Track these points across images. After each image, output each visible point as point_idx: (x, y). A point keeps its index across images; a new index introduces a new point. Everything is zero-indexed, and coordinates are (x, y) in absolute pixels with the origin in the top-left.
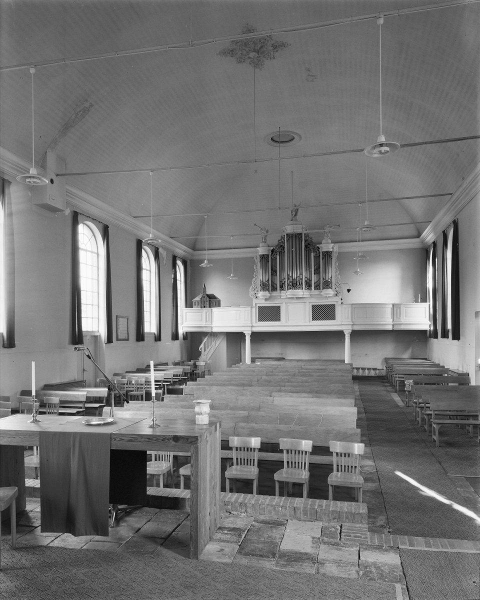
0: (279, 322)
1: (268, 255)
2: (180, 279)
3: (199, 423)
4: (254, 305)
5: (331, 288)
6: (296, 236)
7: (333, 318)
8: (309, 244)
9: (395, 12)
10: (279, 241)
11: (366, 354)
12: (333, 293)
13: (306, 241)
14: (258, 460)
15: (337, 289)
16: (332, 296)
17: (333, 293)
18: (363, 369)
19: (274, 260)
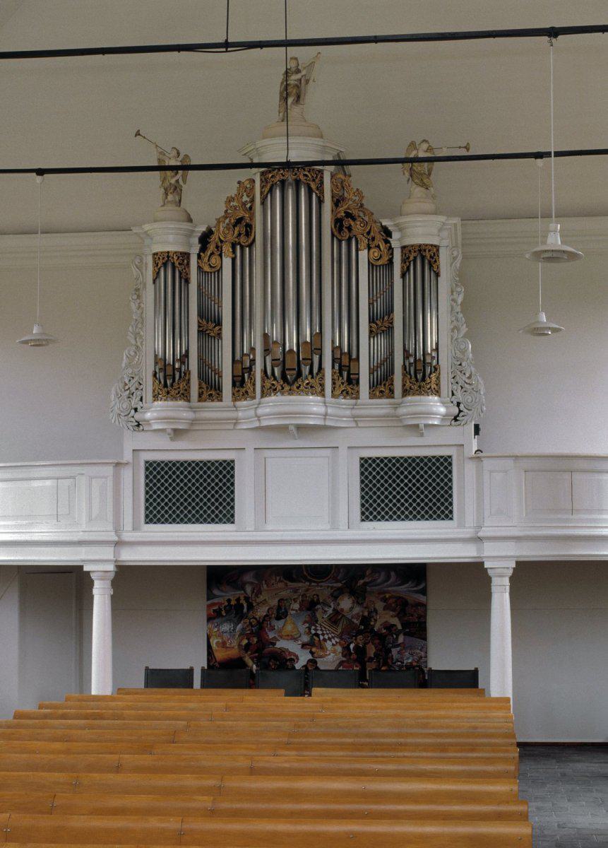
1: (185, 256)
4: (128, 456)
8: (348, 215)
12: (442, 410)
15: (459, 396)
17: (442, 410)
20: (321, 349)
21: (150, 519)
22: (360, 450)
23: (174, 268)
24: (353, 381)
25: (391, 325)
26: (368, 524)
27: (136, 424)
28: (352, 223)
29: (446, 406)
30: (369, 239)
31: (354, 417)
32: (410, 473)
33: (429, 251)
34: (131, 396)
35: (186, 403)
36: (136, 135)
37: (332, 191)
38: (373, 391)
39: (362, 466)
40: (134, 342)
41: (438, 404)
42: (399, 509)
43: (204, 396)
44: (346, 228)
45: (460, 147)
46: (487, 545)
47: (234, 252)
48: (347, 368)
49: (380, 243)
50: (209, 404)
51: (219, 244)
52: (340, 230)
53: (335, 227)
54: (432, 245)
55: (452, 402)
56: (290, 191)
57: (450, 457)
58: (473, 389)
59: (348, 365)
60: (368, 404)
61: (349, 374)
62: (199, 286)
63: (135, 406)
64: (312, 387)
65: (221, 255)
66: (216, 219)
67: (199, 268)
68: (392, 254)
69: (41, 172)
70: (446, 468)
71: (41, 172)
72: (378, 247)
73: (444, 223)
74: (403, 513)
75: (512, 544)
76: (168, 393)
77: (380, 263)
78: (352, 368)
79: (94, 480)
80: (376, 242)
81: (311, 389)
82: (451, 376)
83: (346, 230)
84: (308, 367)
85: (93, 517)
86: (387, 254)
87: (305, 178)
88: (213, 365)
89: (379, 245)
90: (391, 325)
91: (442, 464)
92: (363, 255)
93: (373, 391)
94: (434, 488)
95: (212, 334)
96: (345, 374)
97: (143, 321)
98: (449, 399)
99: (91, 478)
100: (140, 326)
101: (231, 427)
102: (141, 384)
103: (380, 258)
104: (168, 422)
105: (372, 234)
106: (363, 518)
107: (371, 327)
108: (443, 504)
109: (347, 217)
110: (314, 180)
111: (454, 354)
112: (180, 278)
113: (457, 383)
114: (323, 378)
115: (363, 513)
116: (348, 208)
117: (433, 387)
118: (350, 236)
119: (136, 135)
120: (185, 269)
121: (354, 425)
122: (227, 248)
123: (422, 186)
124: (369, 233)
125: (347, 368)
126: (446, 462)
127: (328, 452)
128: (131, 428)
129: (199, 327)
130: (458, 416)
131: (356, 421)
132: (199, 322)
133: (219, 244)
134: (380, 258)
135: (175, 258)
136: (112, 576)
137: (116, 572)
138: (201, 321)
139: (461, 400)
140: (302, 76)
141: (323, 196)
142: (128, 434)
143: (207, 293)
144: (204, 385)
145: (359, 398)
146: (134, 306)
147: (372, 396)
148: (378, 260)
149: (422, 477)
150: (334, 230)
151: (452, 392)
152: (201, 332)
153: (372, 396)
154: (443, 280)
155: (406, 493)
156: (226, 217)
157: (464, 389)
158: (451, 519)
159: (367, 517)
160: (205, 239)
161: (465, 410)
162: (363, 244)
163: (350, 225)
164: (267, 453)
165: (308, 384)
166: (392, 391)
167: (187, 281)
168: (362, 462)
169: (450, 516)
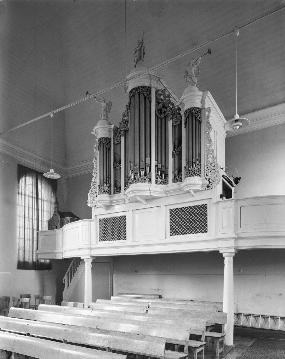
1: (110, 139)
2: (41, 209)
5: (199, 175)
6: (139, 93)
7: (203, 228)
8: (164, 107)
9: (173, 59)
11: (280, 295)
13: (158, 103)
14: (234, 326)
15: (210, 176)
16: (199, 188)
17: (201, 183)
18: (274, 318)
19: (117, 145)
21: (101, 240)
22: (169, 206)
25: (181, 150)
26: (173, 236)
28: (165, 110)
33: (195, 110)
36: (87, 94)
39: (171, 213)
44: (163, 112)
45: (206, 53)
48: (160, 169)
50: (117, 194)
52: (161, 113)
53: (158, 112)
55: (206, 179)
60: (171, 186)
64: (144, 179)
67: (114, 143)
68: (182, 119)
72: (176, 117)
76: (101, 191)
77: (177, 124)
78: (162, 169)
82: (206, 167)
89: (176, 116)
90: (181, 150)
96: (163, 175)
106: (171, 234)
108: (203, 226)
110: (146, 92)
112: (106, 148)
115: (171, 232)
119: (87, 94)
120: (108, 144)
121: (166, 196)
125: (160, 169)
127: (157, 208)
130: (209, 185)
131: (166, 194)
136: (233, 255)
137: (236, 254)
141: (151, 99)
145: (168, 184)
152: (115, 168)
157: (211, 172)
166: (181, 179)
168: (171, 211)
169: (206, 231)
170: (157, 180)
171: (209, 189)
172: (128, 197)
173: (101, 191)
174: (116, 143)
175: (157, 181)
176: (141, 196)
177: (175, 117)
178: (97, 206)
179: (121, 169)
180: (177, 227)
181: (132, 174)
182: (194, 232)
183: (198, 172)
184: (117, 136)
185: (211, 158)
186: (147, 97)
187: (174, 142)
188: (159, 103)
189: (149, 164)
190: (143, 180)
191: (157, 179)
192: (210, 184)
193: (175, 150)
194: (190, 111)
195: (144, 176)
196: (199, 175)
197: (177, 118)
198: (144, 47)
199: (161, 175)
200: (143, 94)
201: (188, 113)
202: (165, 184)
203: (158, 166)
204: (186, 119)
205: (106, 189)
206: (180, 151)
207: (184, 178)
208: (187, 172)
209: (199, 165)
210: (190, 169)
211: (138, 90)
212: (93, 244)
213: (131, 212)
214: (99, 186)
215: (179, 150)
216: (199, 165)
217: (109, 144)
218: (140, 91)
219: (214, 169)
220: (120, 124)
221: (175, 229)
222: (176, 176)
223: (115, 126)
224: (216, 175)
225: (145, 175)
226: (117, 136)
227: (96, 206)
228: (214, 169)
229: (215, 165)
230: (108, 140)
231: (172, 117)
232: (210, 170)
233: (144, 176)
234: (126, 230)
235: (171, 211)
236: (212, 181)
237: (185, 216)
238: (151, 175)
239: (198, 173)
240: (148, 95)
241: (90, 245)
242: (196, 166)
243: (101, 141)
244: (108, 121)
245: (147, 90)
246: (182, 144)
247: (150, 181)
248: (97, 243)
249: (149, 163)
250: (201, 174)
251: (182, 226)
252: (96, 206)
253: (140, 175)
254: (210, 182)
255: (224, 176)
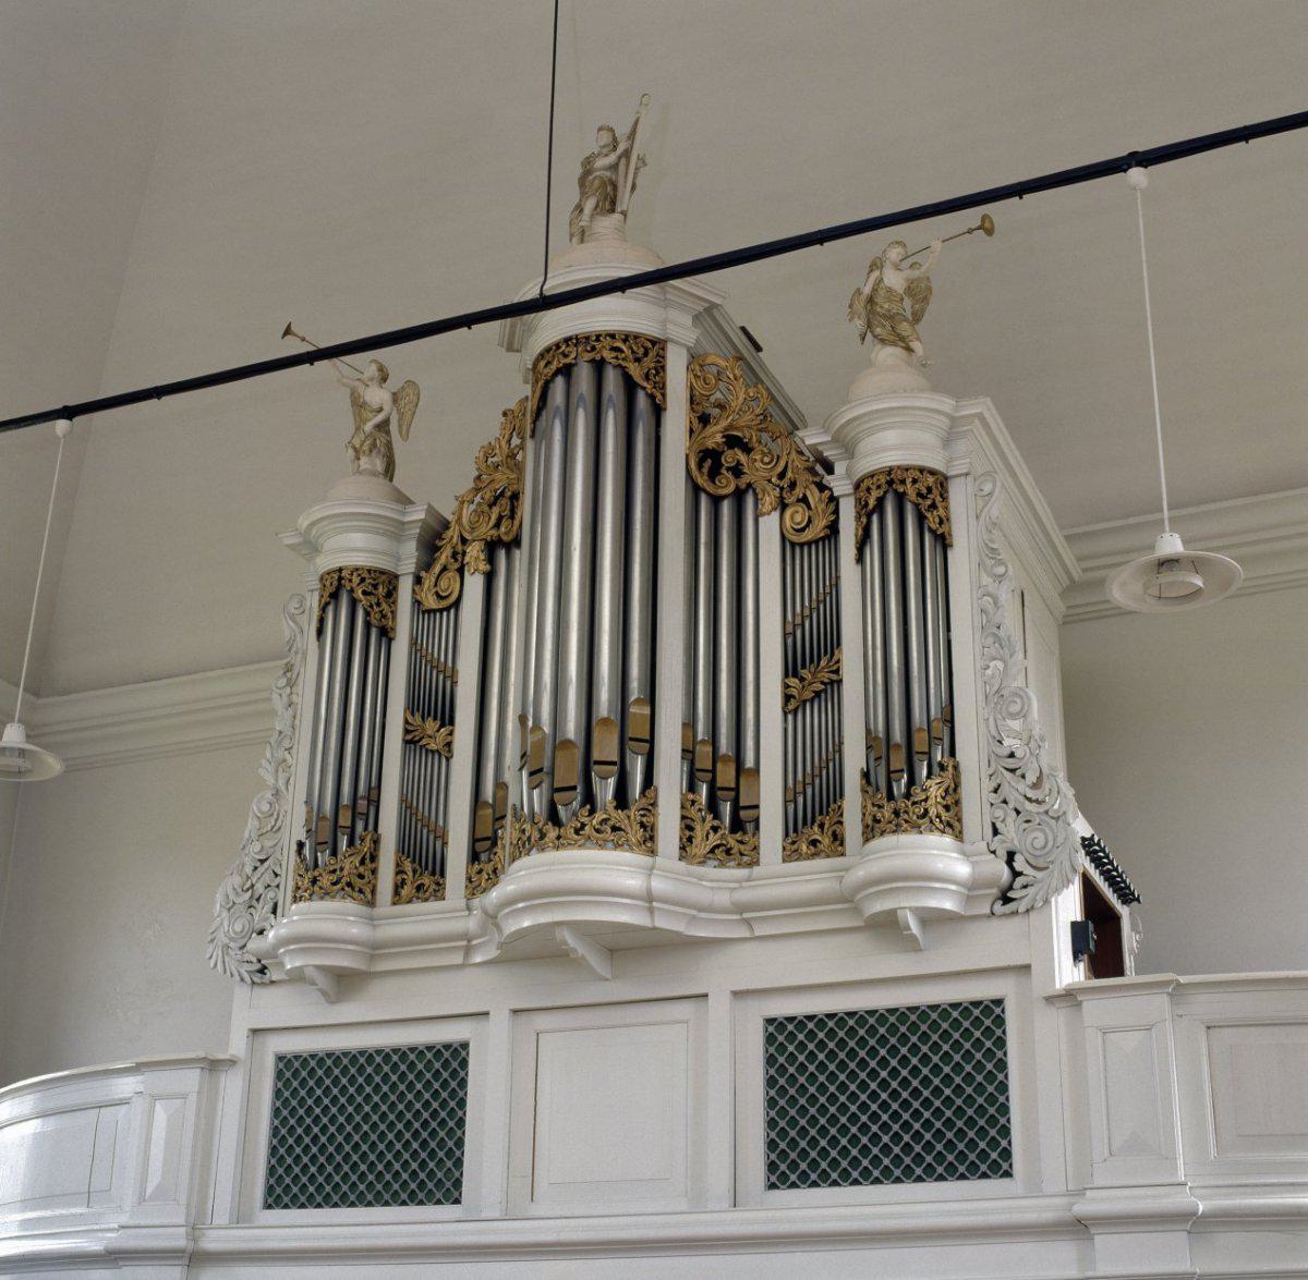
0: (447, 1211)
1: (392, 580)
3: (180, 1268)
4: (237, 1045)
5: (952, 824)
6: (599, 366)
8: (733, 441)
10: (488, 452)
12: (962, 869)
15: (1011, 832)
17: (962, 869)
20: (651, 741)
21: (277, 1197)
23: (353, 603)
24: (744, 822)
25: (834, 677)
26: (785, 1196)
27: (258, 966)
28: (743, 458)
29: (972, 863)
30: (782, 489)
31: (740, 908)
32: (893, 1051)
33: (915, 481)
34: (254, 903)
35: (364, 909)
37: (692, 389)
38: (794, 843)
39: (770, 1039)
40: (270, 780)
41: (955, 855)
42: (865, 1150)
43: (404, 892)
44: (728, 469)
45: (970, 231)
46: (1103, 1241)
47: (491, 560)
49: (808, 494)
51: (460, 548)
52: (714, 474)
53: (700, 466)
54: (922, 470)
55: (994, 852)
56: (611, 414)
57: (999, 1002)
58: (1047, 812)
59: (733, 785)
61: (736, 809)
62: (414, 642)
63: (258, 927)
64: (615, 829)
65: (461, 571)
66: (457, 498)
67: (417, 603)
68: (836, 512)
69: (69, 413)
70: (988, 1032)
71: (69, 413)
72: (804, 500)
73: (953, 419)
74: (876, 1161)
75: (1178, 1238)
76: (314, 881)
77: (808, 536)
79: (157, 1103)
80: (799, 492)
81: (614, 835)
83: (729, 475)
84: (612, 781)
85: (149, 1191)
86: (824, 512)
87: (614, 354)
88: (433, 818)
89: (805, 496)
90: (834, 677)
91: (977, 1022)
92: (770, 526)
93: (794, 843)
94: (958, 1090)
95: (433, 746)
96: (727, 808)
97: (294, 734)
98: (983, 845)
99: (155, 1098)
100: (286, 744)
101: (458, 959)
102: (276, 875)
103: (807, 525)
104: (302, 950)
105: (789, 474)
106: (773, 1179)
107: (786, 686)
109: (731, 447)
110: (638, 360)
111: (994, 732)
112: (368, 625)
113: (1005, 802)
114: (651, 808)
116: (731, 427)
117: (932, 812)
118: (737, 487)
120: (378, 604)
122: (475, 552)
123: (894, 344)
124: (782, 476)
126: (990, 1014)
128: (246, 977)
129: (407, 732)
132: (406, 722)
133: (460, 548)
134: (807, 525)
135: (356, 580)
138: (410, 719)
139: (1016, 845)
140: (620, 158)
141: (664, 395)
142: (242, 993)
143: (429, 658)
144: (408, 866)
145: (757, 863)
146: (279, 704)
147: (791, 853)
148: (803, 530)
149: (925, 1059)
150: (695, 472)
151: (994, 825)
152: (411, 741)
153: (791, 853)
154: (961, 559)
155: (884, 1106)
156: (477, 490)
157: (1022, 817)
158: (1008, 1174)
159: (783, 1178)
160: (432, 541)
161: (1028, 870)
162: (769, 500)
163: (739, 463)
164: (542, 1021)
165: (605, 821)
166: (838, 838)
167: (386, 634)
168: (771, 1029)
169: (1005, 1166)
170: (690, 839)
171: (1015, 913)
172: (498, 926)
173: (314, 881)
174: (431, 602)
175: (686, 843)
176: (583, 929)
177: (799, 500)
178: (273, 974)
179: (450, 751)
180: (328, 1082)
181: (536, 792)
182: (924, 1171)
183: (947, 808)
184: (437, 569)
185: (1017, 736)
186: (644, 388)
187: (790, 629)
188: (704, 420)
189: (707, 771)
190: (608, 835)
191: (690, 828)
192: (1020, 881)
193: (795, 674)
194: (890, 483)
195: (616, 808)
196: (950, 825)
197: (809, 508)
198: (642, 161)
199: (713, 807)
200: (619, 371)
201: (875, 494)
202: (739, 865)
203: (693, 752)
204: (864, 520)
205: (350, 864)
206: (832, 682)
207: (861, 839)
208: (880, 807)
209: (950, 768)
210: (899, 787)
211: (593, 348)
212: (217, 1221)
213: (500, 1022)
214: (301, 845)
215: (826, 676)
216: (950, 768)
217: (384, 606)
218: (608, 355)
219: (1037, 801)
220: (462, 503)
221: (376, 1099)
222: (805, 823)
223: (430, 510)
224: (1050, 838)
225: (622, 799)
226: (437, 569)
227: (262, 971)
228: (1037, 801)
229: (1040, 778)
230: (382, 583)
231: (782, 498)
232: (1011, 805)
233: (616, 808)
234: (274, 1136)
235: (771, 1029)
236: (1028, 870)
237: (863, 1064)
238: (654, 804)
239: (945, 815)
240: (647, 377)
241: (195, 1228)
242: (929, 776)
243: (339, 587)
244: (391, 480)
245: (646, 354)
246: (839, 644)
247: (652, 838)
248: (240, 1218)
249: (648, 737)
250: (959, 820)
251: (813, 1121)
252: (262, 971)
253: (589, 798)
254: (1016, 874)
255: (1087, 844)
